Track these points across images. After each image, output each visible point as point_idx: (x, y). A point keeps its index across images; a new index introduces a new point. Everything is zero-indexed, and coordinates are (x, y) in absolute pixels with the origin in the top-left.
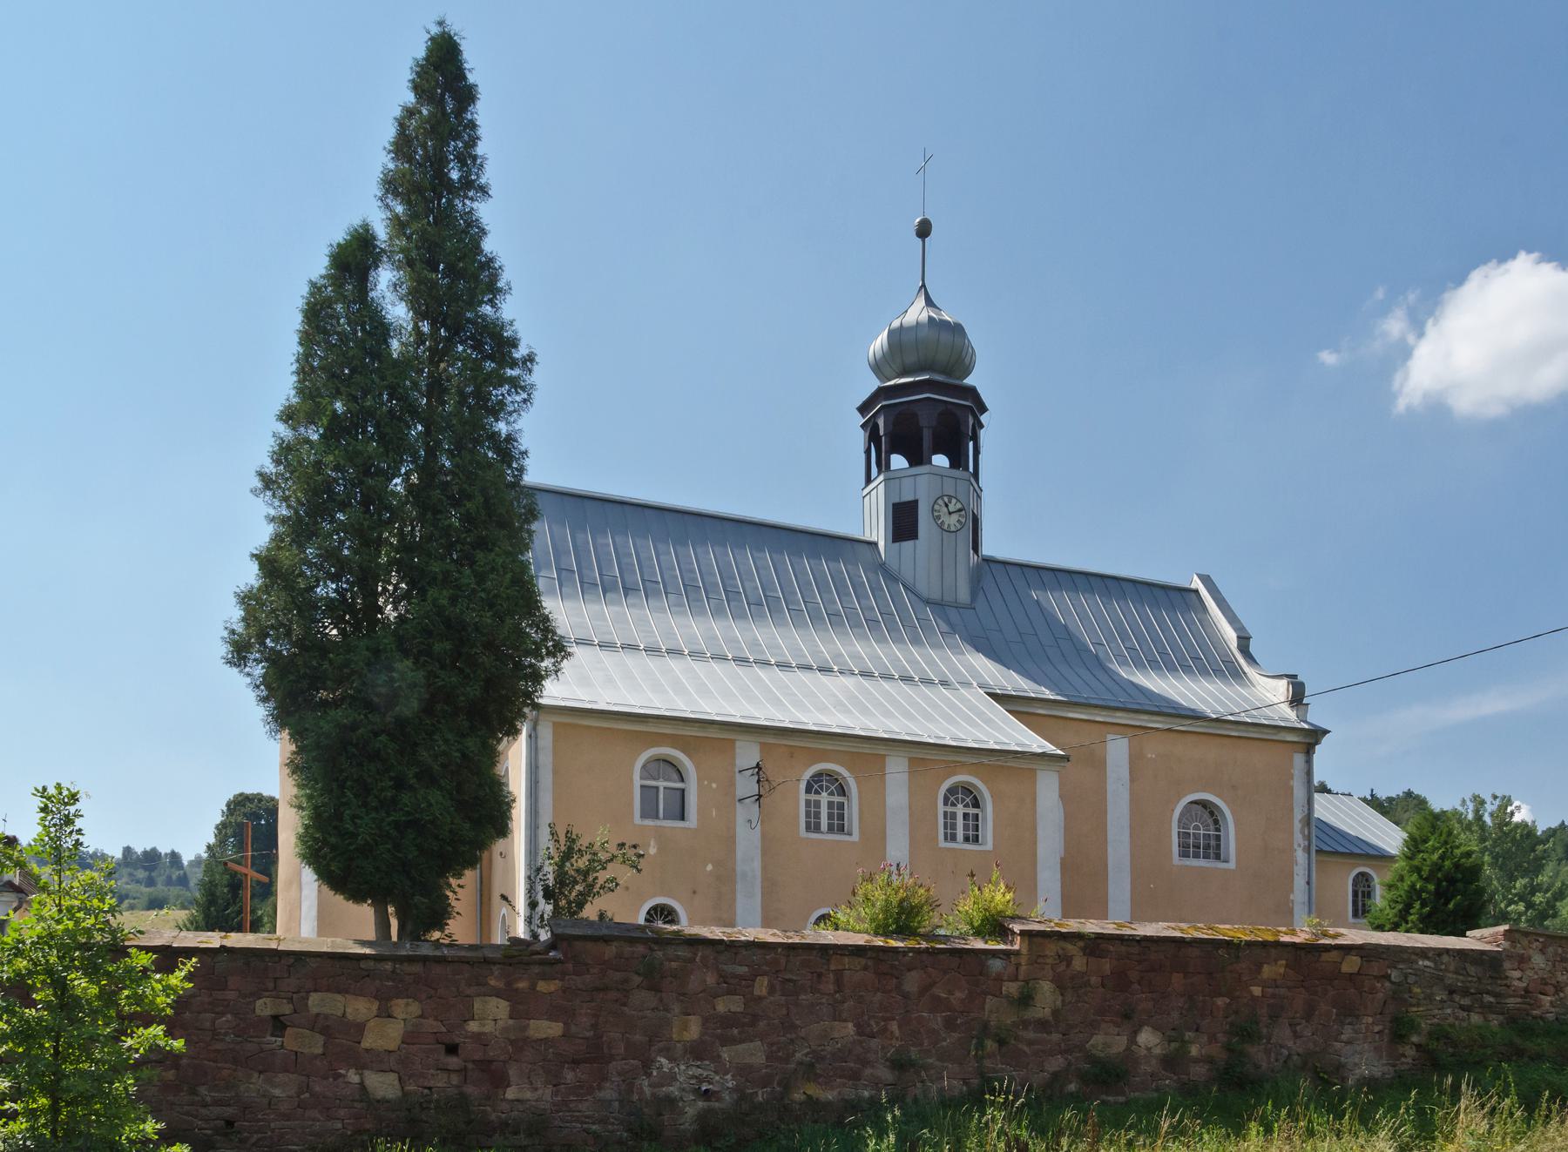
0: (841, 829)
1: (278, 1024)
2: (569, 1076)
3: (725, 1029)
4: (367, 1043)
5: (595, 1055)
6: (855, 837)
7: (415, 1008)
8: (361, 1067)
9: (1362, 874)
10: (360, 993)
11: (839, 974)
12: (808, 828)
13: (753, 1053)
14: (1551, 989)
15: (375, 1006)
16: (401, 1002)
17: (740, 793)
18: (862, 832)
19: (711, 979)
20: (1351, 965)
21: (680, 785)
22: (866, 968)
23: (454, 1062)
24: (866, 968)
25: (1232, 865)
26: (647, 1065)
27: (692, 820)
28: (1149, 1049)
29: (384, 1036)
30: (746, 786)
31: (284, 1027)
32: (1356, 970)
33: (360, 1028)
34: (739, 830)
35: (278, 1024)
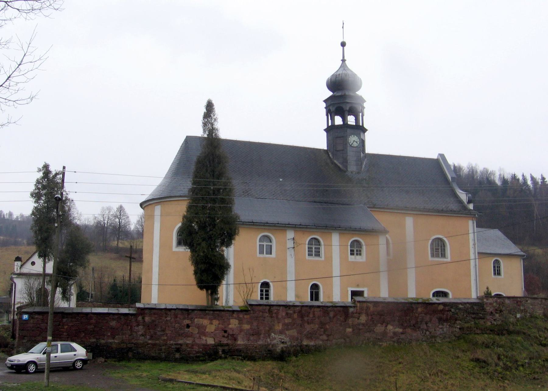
0: (319, 255)
1: (188, 326)
2: (252, 338)
3: (287, 327)
4: (207, 331)
5: (257, 333)
6: (323, 259)
7: (217, 322)
8: (205, 336)
9: (496, 260)
10: (206, 319)
11: (314, 312)
12: (309, 255)
14: (498, 312)
15: (209, 322)
16: (214, 321)
19: (284, 314)
20: (441, 307)
21: (270, 244)
25: (449, 260)
26: (269, 335)
27: (274, 255)
29: (211, 328)
30: (290, 244)
33: (206, 327)
34: (288, 258)
35: (188, 326)
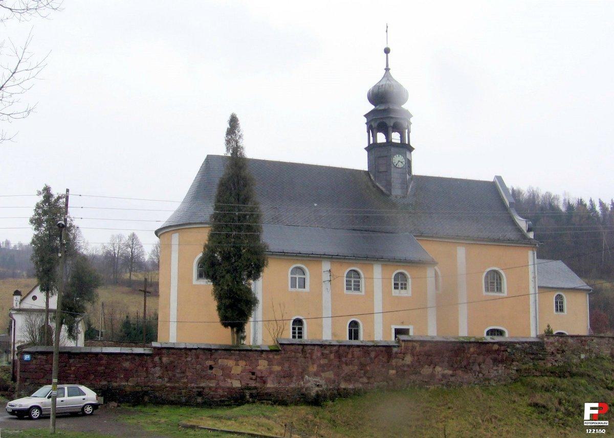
1: (211, 368)
3: (323, 368)
4: (232, 372)
5: (288, 375)
7: (244, 363)
9: (559, 295)
10: (231, 359)
13: (330, 375)
14: (560, 352)
17: (323, 280)
18: (366, 292)
20: (496, 347)
21: (303, 276)
22: (360, 351)
23: (254, 377)
24: (360, 351)
26: (303, 378)
28: (438, 372)
30: (326, 277)
31: (213, 368)
32: (497, 349)
33: (231, 369)
34: (324, 293)
35: (211, 368)
